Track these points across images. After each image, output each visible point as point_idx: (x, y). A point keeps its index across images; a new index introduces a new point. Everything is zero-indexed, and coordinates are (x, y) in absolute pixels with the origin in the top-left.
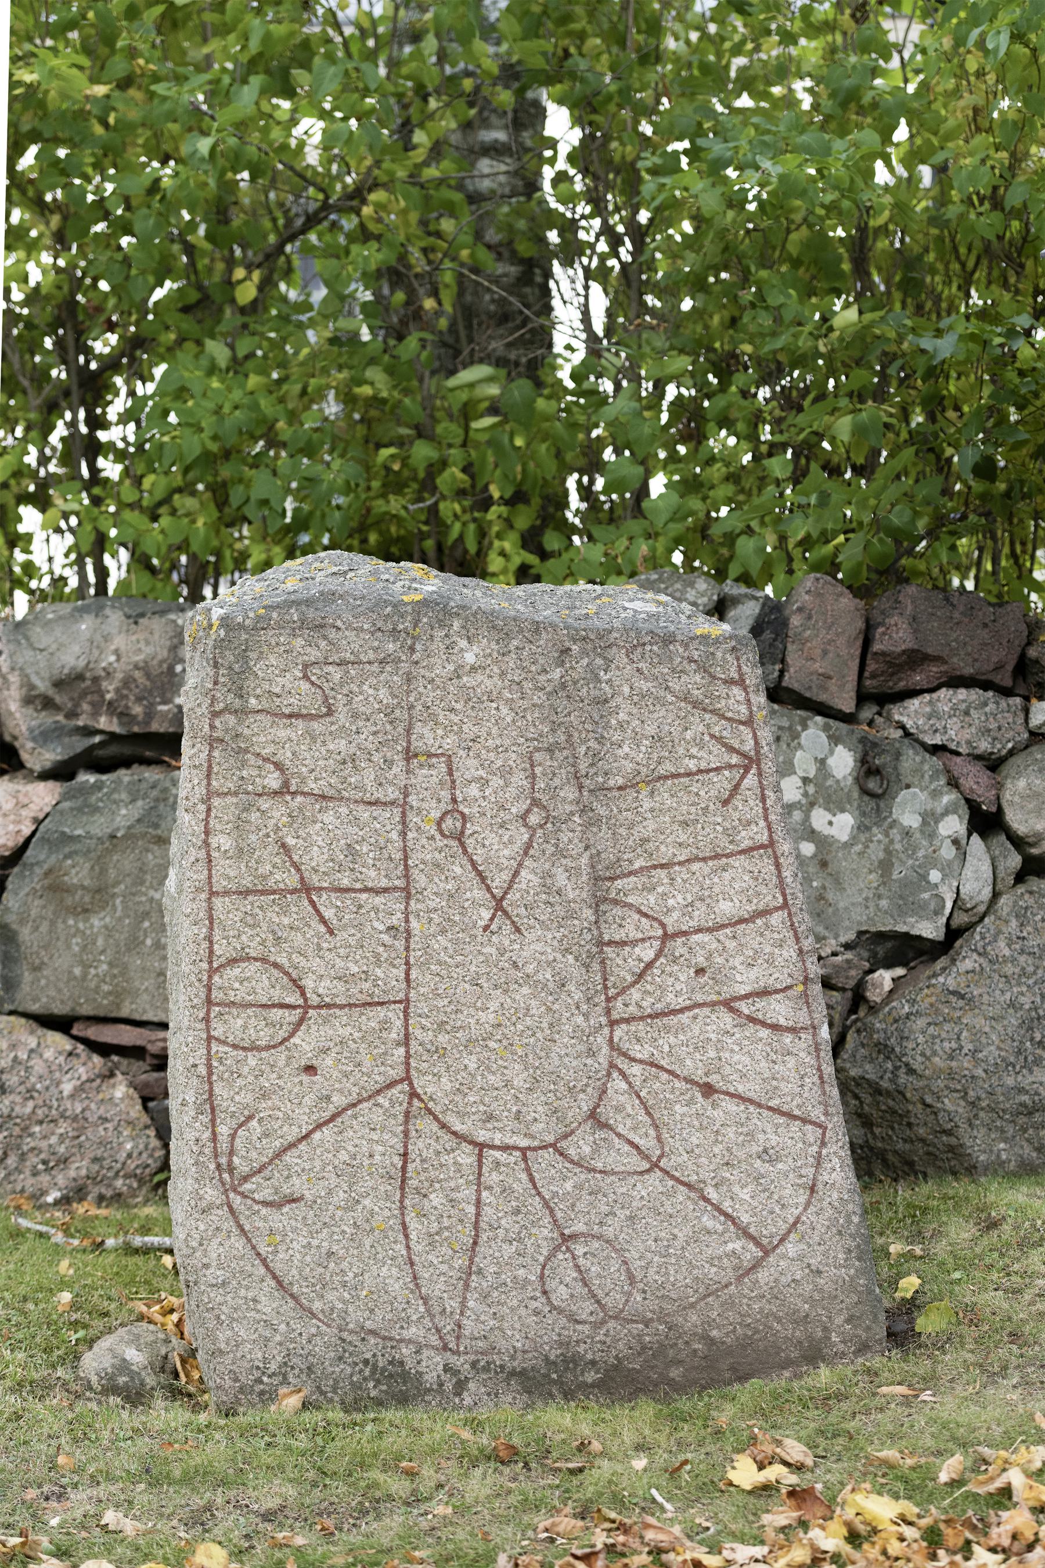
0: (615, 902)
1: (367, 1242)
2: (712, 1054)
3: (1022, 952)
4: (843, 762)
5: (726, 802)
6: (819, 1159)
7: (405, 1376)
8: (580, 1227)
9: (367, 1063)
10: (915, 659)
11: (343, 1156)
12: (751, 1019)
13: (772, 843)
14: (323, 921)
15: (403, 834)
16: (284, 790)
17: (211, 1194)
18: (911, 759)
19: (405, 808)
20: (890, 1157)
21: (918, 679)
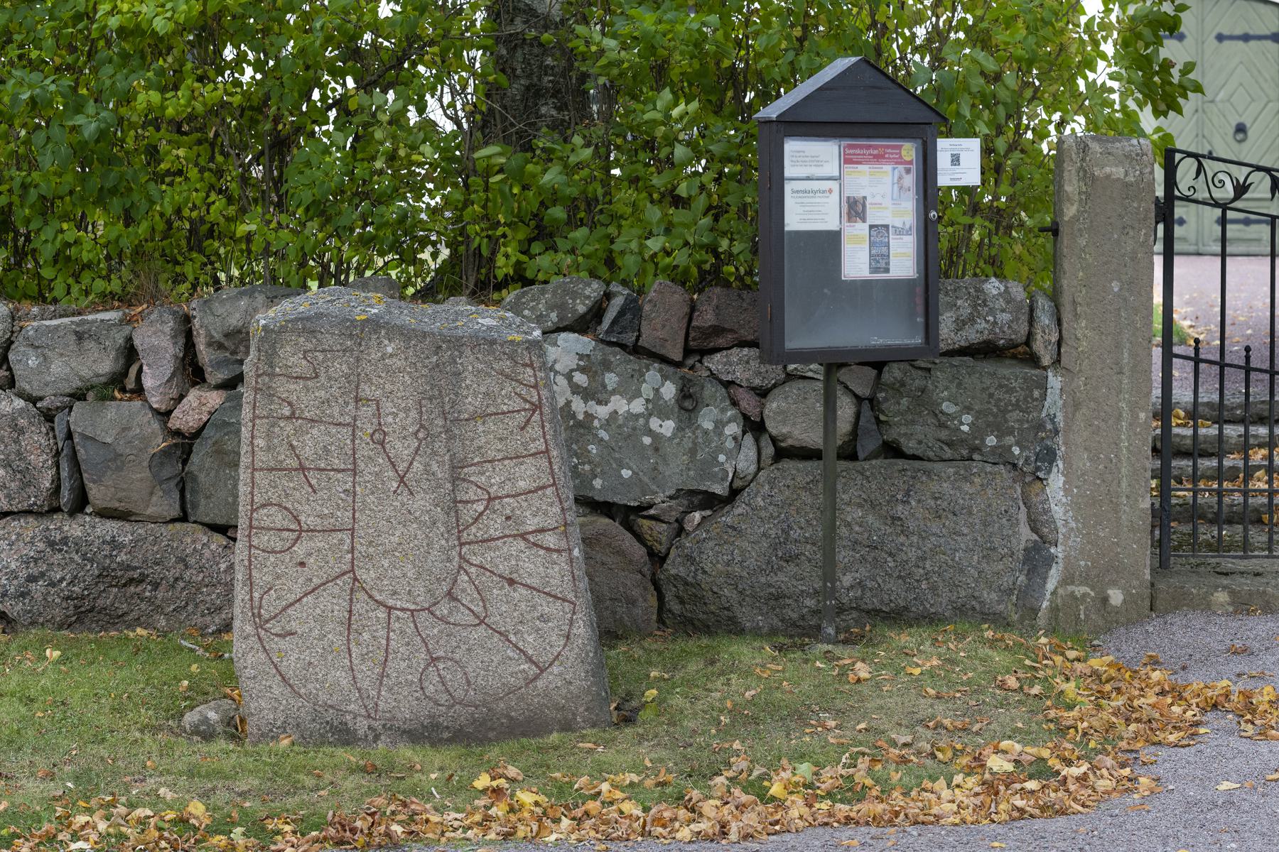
0: (464, 480)
1: (330, 658)
2: (514, 562)
3: (771, 504)
4: (669, 391)
5: (522, 429)
6: (571, 622)
7: (348, 731)
8: (441, 653)
9: (332, 562)
10: (717, 330)
11: (318, 611)
12: (535, 544)
13: (547, 451)
14: (311, 486)
15: (353, 441)
16: (292, 417)
17: (249, 629)
18: (710, 390)
19: (354, 427)
20: (696, 622)
21: (721, 342)
